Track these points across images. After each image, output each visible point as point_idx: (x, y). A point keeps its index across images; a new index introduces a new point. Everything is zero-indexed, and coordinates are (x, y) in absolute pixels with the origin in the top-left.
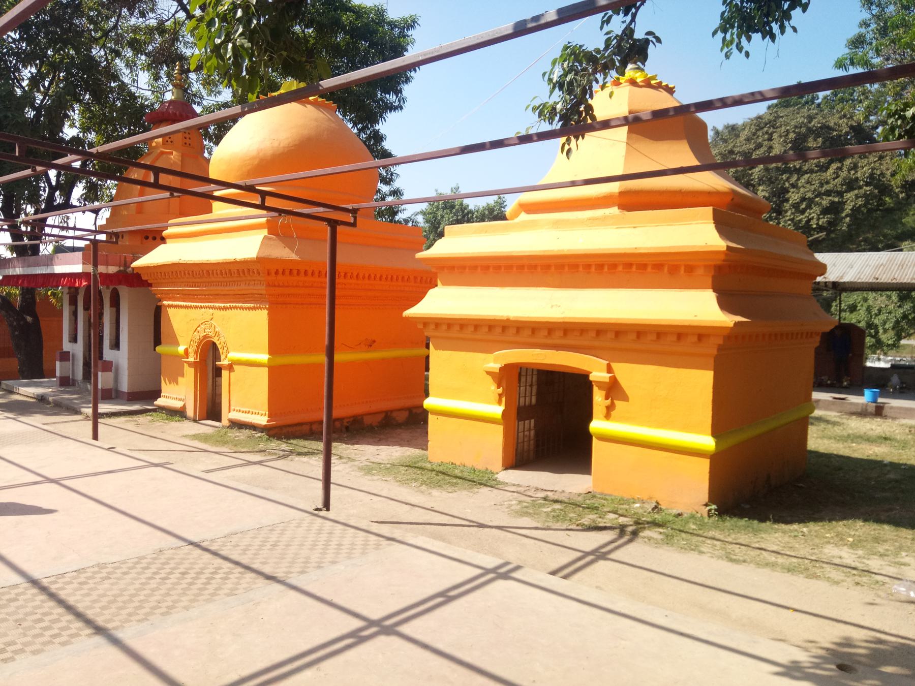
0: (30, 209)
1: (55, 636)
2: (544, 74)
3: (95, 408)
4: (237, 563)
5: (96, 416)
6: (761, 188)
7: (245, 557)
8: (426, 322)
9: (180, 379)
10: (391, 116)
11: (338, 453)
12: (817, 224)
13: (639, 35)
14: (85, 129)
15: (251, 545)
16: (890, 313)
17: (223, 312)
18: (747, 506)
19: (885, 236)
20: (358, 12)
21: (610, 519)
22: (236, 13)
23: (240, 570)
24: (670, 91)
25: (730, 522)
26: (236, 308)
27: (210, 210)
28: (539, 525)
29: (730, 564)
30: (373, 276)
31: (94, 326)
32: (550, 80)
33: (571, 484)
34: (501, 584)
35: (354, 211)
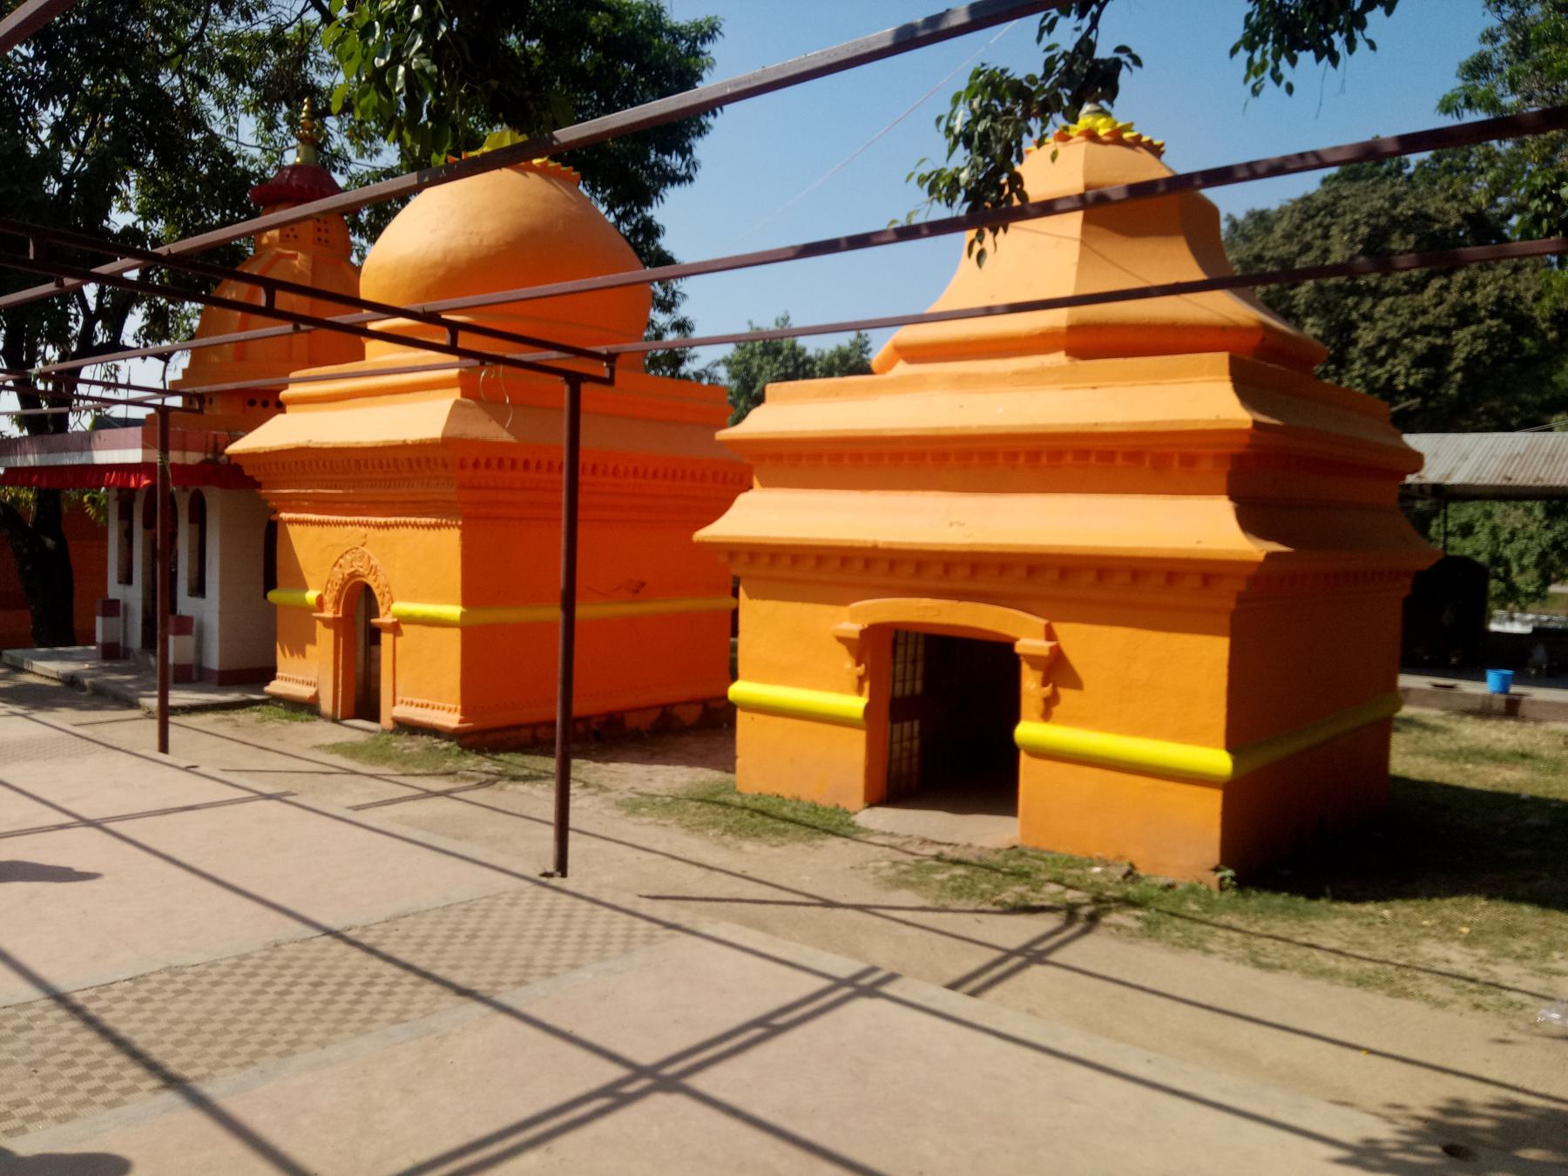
0: (52, 353)
3: (164, 698)
4: (408, 967)
5: (165, 712)
6: (1310, 321)
9: (309, 649)
10: (672, 193)
11: (581, 776)
12: (1406, 384)
13: (1103, 51)
14: (147, 214)
16: (1531, 538)
17: (382, 533)
19: (1523, 405)
21: (1051, 892)
23: (413, 978)
24: (1156, 150)
25: (1256, 900)
26: (406, 525)
27: (360, 356)
28: (928, 903)
29: (1257, 972)
30: (641, 471)
31: (161, 556)
32: (949, 130)
33: (984, 832)
34: (864, 1005)
35: (611, 358)
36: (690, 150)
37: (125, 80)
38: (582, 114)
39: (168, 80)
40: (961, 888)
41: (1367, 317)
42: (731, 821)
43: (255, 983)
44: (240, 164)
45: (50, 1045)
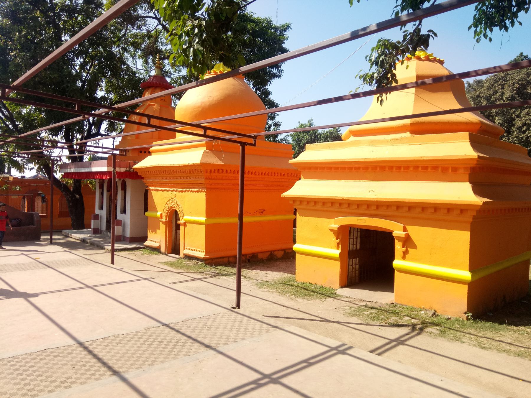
0: (79, 136)
1: (92, 375)
2: (366, 57)
3: (113, 246)
4: (190, 337)
5: (113, 251)
6: (497, 118)
7: (194, 333)
8: (294, 200)
9: (158, 231)
10: (274, 81)
11: (244, 275)
13: (424, 32)
14: (108, 92)
15: (197, 327)
17: (181, 194)
18: (491, 314)
20: (257, 22)
21: (406, 320)
22: (194, 31)
23: (191, 341)
24: (441, 62)
25: (480, 324)
26: (188, 191)
27: (175, 137)
28: (362, 322)
29: (481, 350)
30: (264, 173)
31: (112, 202)
32: (370, 60)
33: (381, 298)
34: (340, 357)
35: (255, 137)
36: (280, 67)
37: (102, 50)
38: (249, 62)
39: (115, 49)
40: (374, 317)
41: (518, 116)
42: (294, 291)
43: (141, 341)
44: (137, 75)
45: (78, 359)
